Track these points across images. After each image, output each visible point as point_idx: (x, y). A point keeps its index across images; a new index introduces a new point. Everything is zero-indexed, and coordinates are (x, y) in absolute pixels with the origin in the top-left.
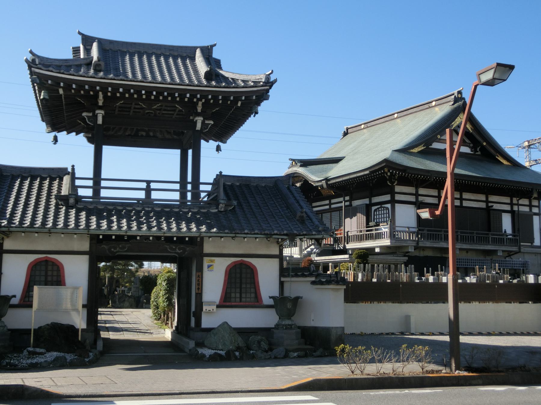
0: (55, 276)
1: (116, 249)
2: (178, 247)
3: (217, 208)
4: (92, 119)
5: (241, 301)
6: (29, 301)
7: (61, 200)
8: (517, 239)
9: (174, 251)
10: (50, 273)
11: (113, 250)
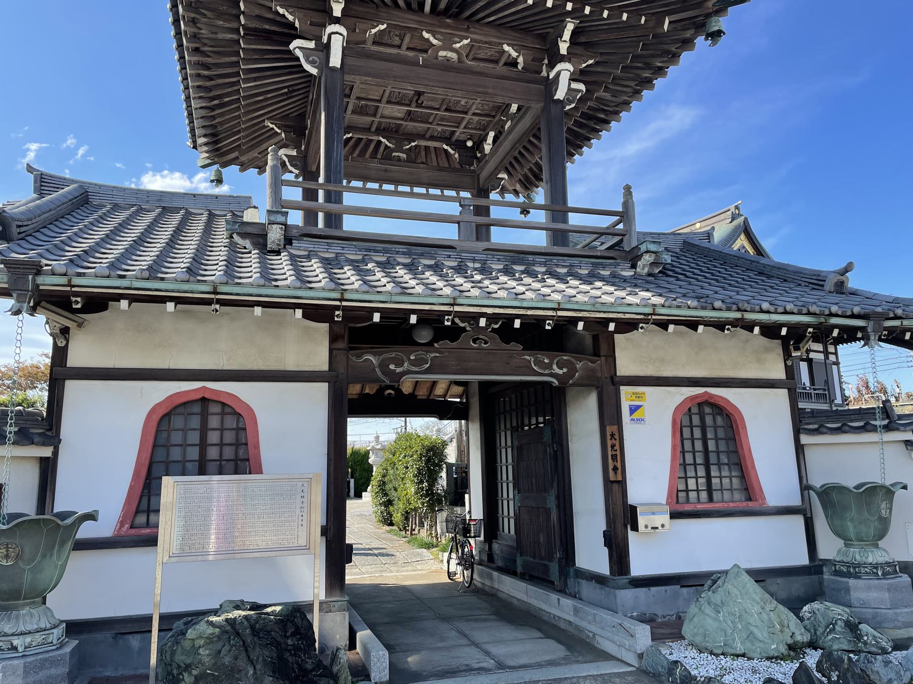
1: (402, 365)
2: (555, 361)
3: (634, 266)
4: (316, 58)
5: (711, 499)
7: (243, 235)
8: (826, 394)
9: (547, 372)
10: (213, 437)
11: (392, 367)
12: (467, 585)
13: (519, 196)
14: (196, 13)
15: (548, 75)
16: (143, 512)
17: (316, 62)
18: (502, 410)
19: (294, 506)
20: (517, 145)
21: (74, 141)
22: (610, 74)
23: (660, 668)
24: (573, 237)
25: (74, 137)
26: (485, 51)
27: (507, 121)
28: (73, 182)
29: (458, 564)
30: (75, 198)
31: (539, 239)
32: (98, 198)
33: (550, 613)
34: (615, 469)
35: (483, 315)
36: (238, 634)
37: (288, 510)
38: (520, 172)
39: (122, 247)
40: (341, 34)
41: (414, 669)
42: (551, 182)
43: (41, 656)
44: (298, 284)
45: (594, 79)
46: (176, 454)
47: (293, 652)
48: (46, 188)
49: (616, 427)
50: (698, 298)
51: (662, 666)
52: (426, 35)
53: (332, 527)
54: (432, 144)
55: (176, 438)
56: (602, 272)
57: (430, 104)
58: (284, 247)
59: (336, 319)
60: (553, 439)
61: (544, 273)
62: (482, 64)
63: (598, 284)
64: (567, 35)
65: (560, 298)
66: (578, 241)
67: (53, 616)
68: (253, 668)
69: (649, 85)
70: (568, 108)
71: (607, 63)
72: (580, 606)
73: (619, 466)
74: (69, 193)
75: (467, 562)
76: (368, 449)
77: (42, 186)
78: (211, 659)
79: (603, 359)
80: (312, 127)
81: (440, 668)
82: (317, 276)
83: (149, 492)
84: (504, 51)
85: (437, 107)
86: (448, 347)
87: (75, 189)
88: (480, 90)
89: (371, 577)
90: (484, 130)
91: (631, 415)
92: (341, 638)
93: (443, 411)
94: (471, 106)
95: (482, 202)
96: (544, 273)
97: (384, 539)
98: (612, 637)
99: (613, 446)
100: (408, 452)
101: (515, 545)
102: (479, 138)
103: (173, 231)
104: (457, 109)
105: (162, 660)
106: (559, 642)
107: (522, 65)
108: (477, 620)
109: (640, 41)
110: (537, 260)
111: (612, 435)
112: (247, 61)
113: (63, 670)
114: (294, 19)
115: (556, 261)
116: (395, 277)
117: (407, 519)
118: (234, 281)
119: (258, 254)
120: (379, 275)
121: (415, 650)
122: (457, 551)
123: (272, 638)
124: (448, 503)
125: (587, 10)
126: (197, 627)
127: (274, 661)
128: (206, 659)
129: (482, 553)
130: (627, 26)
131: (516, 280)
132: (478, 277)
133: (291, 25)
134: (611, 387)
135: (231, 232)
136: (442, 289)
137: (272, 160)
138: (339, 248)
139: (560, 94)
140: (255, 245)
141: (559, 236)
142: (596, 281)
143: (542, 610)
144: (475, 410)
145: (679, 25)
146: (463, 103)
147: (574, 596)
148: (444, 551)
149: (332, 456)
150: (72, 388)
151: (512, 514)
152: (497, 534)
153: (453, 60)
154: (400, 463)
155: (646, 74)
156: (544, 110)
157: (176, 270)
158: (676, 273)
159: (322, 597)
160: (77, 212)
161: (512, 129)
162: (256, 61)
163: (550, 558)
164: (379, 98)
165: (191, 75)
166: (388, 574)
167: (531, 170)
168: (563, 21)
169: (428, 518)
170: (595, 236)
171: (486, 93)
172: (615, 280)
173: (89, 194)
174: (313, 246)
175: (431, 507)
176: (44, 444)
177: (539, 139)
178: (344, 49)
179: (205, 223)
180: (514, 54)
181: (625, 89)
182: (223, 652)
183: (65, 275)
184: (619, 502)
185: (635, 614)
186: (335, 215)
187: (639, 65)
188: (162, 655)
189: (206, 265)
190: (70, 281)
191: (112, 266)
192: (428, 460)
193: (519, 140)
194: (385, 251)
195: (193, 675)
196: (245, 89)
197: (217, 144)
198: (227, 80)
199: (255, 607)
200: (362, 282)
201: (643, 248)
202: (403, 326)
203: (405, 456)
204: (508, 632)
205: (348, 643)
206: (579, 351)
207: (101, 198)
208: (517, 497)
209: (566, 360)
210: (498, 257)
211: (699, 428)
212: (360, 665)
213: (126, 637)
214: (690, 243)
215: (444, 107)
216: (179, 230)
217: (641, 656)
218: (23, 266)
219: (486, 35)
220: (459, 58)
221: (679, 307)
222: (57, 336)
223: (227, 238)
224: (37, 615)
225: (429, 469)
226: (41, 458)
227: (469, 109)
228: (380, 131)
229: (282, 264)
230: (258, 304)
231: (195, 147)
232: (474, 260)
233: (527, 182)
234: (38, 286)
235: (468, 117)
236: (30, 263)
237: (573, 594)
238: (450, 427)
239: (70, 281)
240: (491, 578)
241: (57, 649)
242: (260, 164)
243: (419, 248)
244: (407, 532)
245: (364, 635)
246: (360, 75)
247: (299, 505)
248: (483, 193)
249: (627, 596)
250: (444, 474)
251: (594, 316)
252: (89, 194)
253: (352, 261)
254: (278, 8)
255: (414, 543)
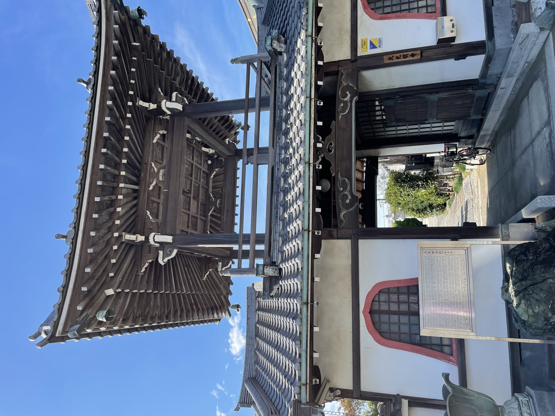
0: (398, 297)
1: (347, 195)
2: (342, 99)
3: (281, 53)
4: (168, 250)
6: (450, 346)
7: (271, 290)
10: (394, 307)
11: (348, 201)
12: (489, 152)
13: (238, 132)
14: (148, 316)
15: (169, 115)
16: (442, 349)
17: (170, 250)
18: (372, 135)
19: (439, 258)
20: (210, 133)
21: (214, 391)
22: (166, 77)
23: (550, 15)
24: (263, 94)
25: (212, 391)
26: (157, 153)
27: (196, 140)
28: (243, 385)
29: (474, 158)
30: (253, 384)
31: (266, 115)
32: (252, 372)
33: (511, 94)
34: (413, 55)
35: (315, 145)
36: (525, 289)
37: (442, 262)
38: (224, 131)
39: (273, 368)
40: (154, 236)
41: (549, 180)
42: (230, 110)
43: (537, 408)
44: (300, 256)
45: (169, 87)
46: (405, 329)
47: (538, 255)
48: (248, 401)
49: (385, 57)
50: (301, 8)
51: (549, 14)
52: (151, 188)
53: (452, 235)
54: (211, 185)
55: (394, 328)
56: (285, 73)
57: (188, 186)
58: (277, 266)
59: (320, 234)
60: (392, 99)
61: (287, 110)
62: (165, 155)
63: (293, 74)
64: (146, 105)
65: (303, 97)
66: (265, 92)
67: (510, 400)
68: (548, 280)
69: (171, 54)
70: (187, 102)
71: (159, 80)
72: (506, 73)
73: (411, 53)
74: (250, 387)
75: (473, 153)
76: (394, 222)
77: (246, 403)
78: (542, 305)
79: (340, 68)
80: (205, 253)
81: (549, 164)
82: (294, 246)
83: (429, 345)
84: (157, 142)
85: (190, 181)
86: (334, 168)
87: (248, 384)
88: (179, 155)
89: (482, 215)
90: (201, 153)
91: (376, 48)
92: (527, 228)
93: (372, 173)
94: (189, 162)
95: (245, 153)
96: (287, 110)
97: (455, 208)
98: (529, 50)
99: (398, 58)
100: (398, 194)
101: (462, 121)
102: (206, 156)
103: (270, 329)
104: (190, 170)
105: (541, 335)
106: (531, 86)
107: (164, 131)
108: (515, 143)
109: (147, 60)
110: (278, 115)
111: (390, 59)
112: (171, 290)
113: (546, 395)
114: (147, 262)
115: (279, 103)
116: (293, 200)
117: (442, 194)
118: (300, 293)
119: (282, 281)
120: (292, 210)
121: (536, 180)
122: (465, 159)
123: (528, 268)
124: (432, 168)
125: (131, 93)
126: (520, 313)
127: (544, 267)
128: (542, 308)
129: (467, 143)
130: (138, 68)
131: (292, 127)
132: (291, 150)
133: (151, 264)
134: (358, 61)
135: (269, 297)
136: (300, 171)
137: (227, 273)
138: (276, 234)
139: (179, 107)
140: (277, 283)
141: (263, 103)
142: (291, 76)
143: (508, 100)
144: (371, 152)
145: (136, 37)
146: (187, 166)
147: (499, 78)
148: (464, 169)
149: (406, 236)
150: (366, 386)
151: (441, 124)
152: (454, 134)
153: (164, 172)
154: (405, 199)
155: (165, 55)
156: (189, 117)
157: (294, 326)
158: (284, 26)
159: (499, 240)
160: (261, 384)
161: (200, 137)
162: (171, 284)
163: (472, 96)
164: (187, 215)
165: (181, 320)
166: (480, 203)
167: (223, 125)
168: (138, 107)
169: (441, 181)
170: (262, 80)
171: (181, 151)
172: (290, 65)
173: (250, 377)
174: (276, 250)
175: (435, 179)
176: (400, 403)
177: (205, 119)
178: (162, 234)
179: (264, 312)
180: (158, 136)
181: (174, 68)
182: (537, 297)
183: (300, 387)
184: (435, 51)
185: (512, 36)
186: (256, 238)
187: (160, 59)
188: (538, 335)
189: (290, 309)
190: (304, 385)
191: (294, 361)
192: (404, 181)
193: (206, 131)
194: (277, 208)
195: (552, 316)
196: (187, 291)
197: (217, 307)
198: (182, 301)
199: (506, 278)
200: (298, 219)
201: (269, 48)
202: (319, 198)
203: (401, 196)
204: (523, 122)
205: (530, 223)
206: (335, 85)
207: (252, 371)
208: (430, 121)
209: (341, 92)
210: (277, 139)
211: (385, 2)
212: (546, 214)
213: (523, 359)
214: (264, 20)
215: (190, 177)
216: (269, 326)
217: (542, 29)
218: (296, 410)
219: (149, 153)
220: (163, 168)
221: (307, 20)
222: (335, 394)
223: (273, 299)
224: (510, 409)
225: (409, 181)
226: (409, 406)
227: (190, 163)
228: (205, 215)
229: (287, 267)
230: (313, 279)
231: (219, 320)
232: (280, 154)
233: (230, 127)
234: (307, 402)
235: (195, 163)
236: (294, 406)
237: (497, 79)
238: (381, 170)
239: (304, 385)
240: (485, 136)
241: (532, 398)
242: (227, 283)
243: (274, 187)
244: (451, 194)
245: (525, 213)
246: (176, 225)
247: (438, 255)
248: (238, 154)
249: (500, 42)
250: (412, 172)
251: (314, 75)
252: (250, 377)
253: (283, 227)
254: (142, 271)
255: (458, 189)
